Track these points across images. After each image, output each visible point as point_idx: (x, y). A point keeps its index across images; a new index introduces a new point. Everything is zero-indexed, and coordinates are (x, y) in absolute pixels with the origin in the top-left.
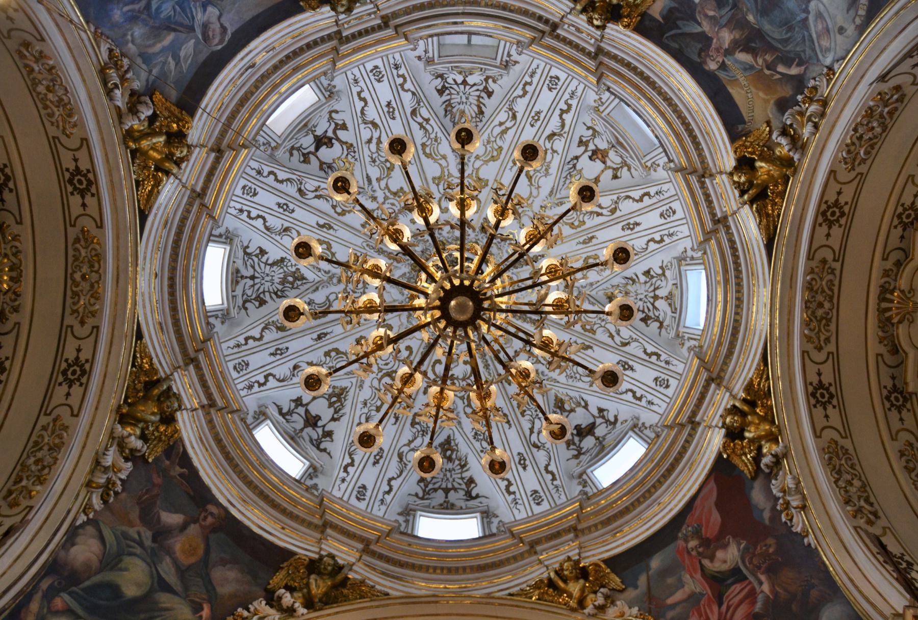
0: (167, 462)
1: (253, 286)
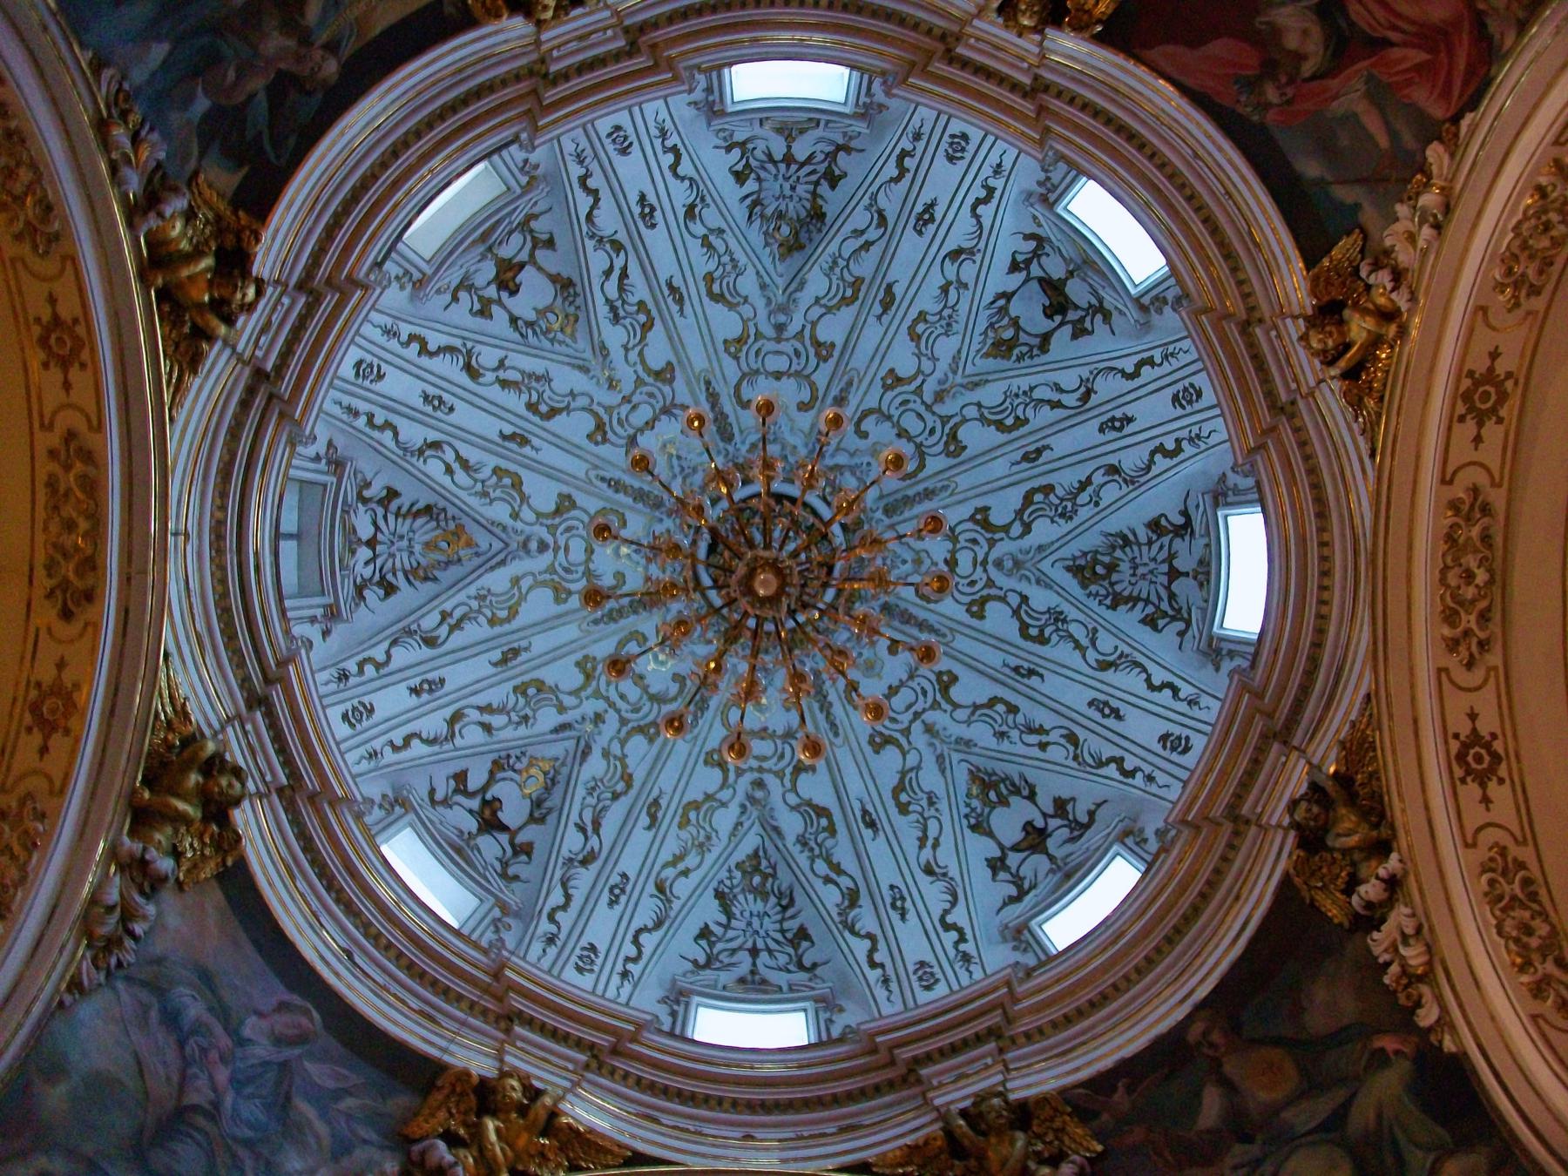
0: (1105, 1117)
1: (770, 951)
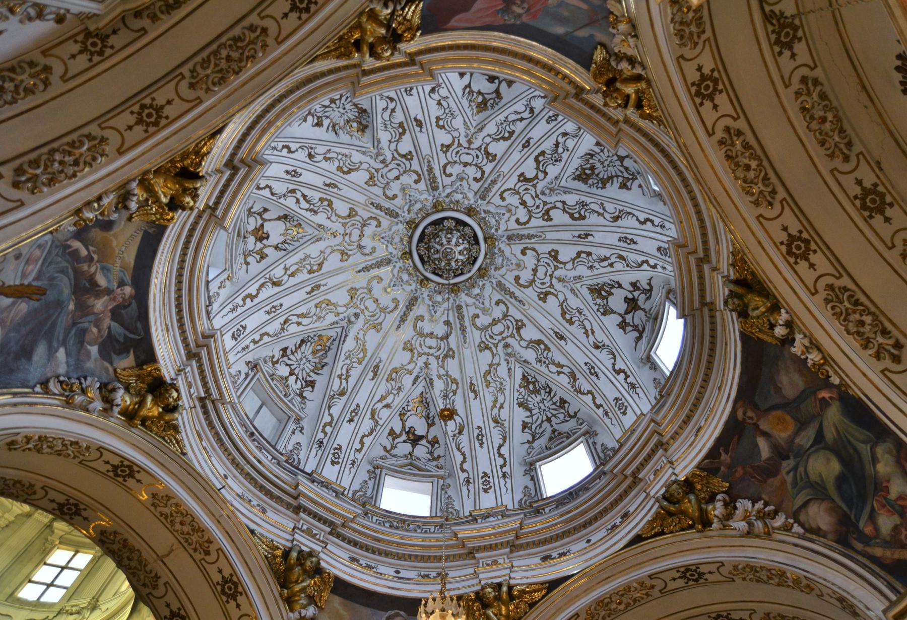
0: (722, 468)
1: (554, 416)
